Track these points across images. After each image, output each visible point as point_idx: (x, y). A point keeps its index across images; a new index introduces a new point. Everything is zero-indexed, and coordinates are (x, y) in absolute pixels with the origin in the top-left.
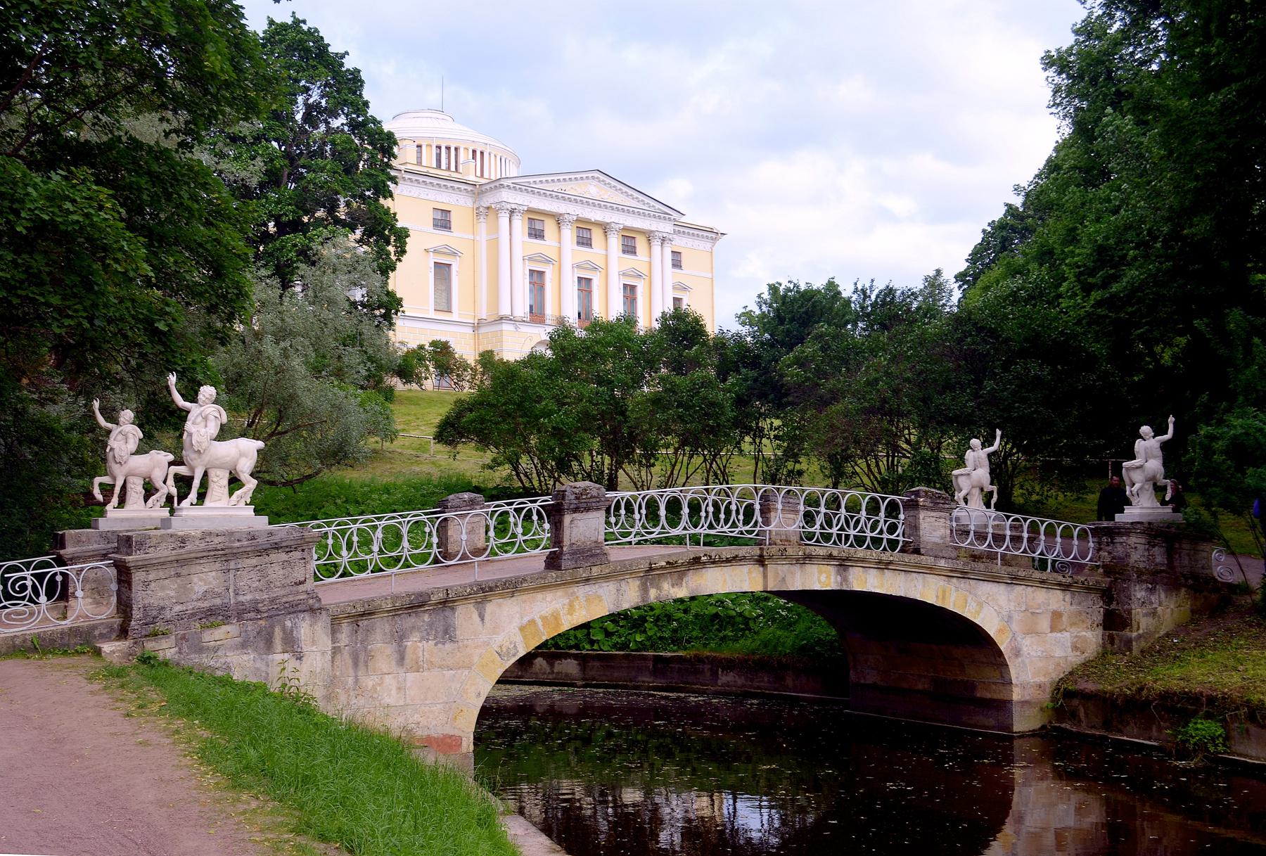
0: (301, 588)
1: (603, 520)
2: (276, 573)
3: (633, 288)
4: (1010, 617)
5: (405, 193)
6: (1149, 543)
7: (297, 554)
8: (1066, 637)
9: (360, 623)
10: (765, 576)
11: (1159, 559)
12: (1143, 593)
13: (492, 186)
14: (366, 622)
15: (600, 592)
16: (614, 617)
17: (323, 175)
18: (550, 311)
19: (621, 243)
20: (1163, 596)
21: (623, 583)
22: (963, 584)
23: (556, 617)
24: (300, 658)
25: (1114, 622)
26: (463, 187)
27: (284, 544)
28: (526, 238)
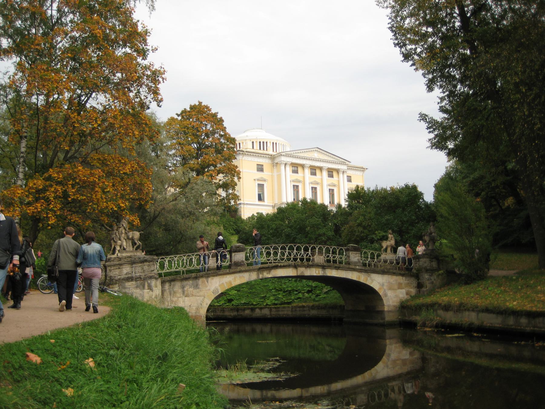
0: (153, 272)
2: (146, 268)
3: (297, 186)
4: (383, 285)
5: (246, 159)
6: (430, 261)
7: (152, 263)
8: (404, 291)
10: (297, 271)
16: (247, 283)
17: (211, 156)
19: (327, 173)
21: (251, 273)
23: (230, 283)
24: (152, 291)
25: (420, 286)
28: (291, 173)
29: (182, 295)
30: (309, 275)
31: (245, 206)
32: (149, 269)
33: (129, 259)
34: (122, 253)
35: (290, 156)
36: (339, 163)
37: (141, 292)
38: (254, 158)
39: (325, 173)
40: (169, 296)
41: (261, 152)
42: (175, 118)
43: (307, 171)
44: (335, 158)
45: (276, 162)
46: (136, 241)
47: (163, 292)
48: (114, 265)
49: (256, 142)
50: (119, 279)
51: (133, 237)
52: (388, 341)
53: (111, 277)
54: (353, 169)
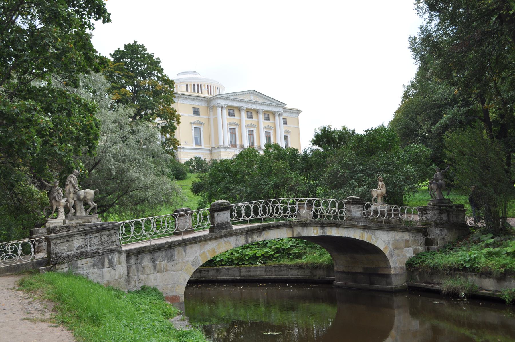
0: (115, 244)
1: (229, 214)
2: (105, 238)
5: (181, 102)
6: (440, 213)
7: (113, 231)
9: (139, 256)
10: (293, 232)
11: (444, 219)
12: (439, 231)
13: (214, 98)
14: (141, 255)
15: (230, 240)
18: (238, 143)
20: (446, 232)
21: (238, 237)
22: (370, 232)
23: (214, 251)
24: (115, 269)
25: (428, 243)
26: (203, 99)
27: (107, 228)
28: (228, 117)
29: (152, 271)
30: (306, 235)
31: (182, 150)
32: (109, 240)
33: (82, 228)
34: (72, 220)
35: (227, 99)
36: (275, 106)
37: (99, 272)
38: (190, 101)
39: (261, 116)
40: (136, 273)
41: (196, 94)
42: (109, 58)
43: (244, 114)
44: (271, 101)
45: (212, 105)
46: (90, 203)
47: (129, 268)
48: (61, 238)
49: (191, 85)
50: (69, 256)
51: (85, 197)
52: (396, 311)
53: (56, 253)
54: (289, 112)
